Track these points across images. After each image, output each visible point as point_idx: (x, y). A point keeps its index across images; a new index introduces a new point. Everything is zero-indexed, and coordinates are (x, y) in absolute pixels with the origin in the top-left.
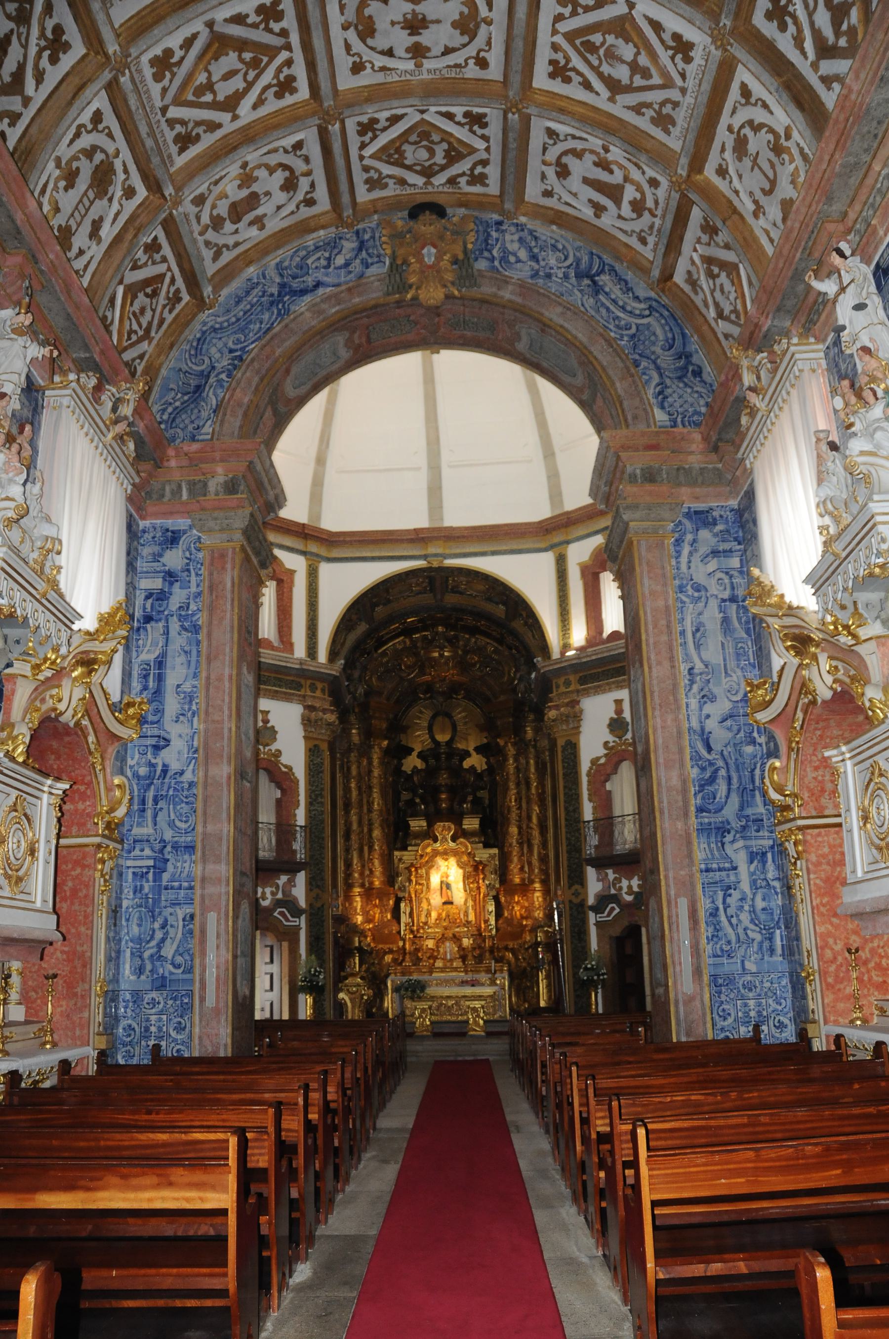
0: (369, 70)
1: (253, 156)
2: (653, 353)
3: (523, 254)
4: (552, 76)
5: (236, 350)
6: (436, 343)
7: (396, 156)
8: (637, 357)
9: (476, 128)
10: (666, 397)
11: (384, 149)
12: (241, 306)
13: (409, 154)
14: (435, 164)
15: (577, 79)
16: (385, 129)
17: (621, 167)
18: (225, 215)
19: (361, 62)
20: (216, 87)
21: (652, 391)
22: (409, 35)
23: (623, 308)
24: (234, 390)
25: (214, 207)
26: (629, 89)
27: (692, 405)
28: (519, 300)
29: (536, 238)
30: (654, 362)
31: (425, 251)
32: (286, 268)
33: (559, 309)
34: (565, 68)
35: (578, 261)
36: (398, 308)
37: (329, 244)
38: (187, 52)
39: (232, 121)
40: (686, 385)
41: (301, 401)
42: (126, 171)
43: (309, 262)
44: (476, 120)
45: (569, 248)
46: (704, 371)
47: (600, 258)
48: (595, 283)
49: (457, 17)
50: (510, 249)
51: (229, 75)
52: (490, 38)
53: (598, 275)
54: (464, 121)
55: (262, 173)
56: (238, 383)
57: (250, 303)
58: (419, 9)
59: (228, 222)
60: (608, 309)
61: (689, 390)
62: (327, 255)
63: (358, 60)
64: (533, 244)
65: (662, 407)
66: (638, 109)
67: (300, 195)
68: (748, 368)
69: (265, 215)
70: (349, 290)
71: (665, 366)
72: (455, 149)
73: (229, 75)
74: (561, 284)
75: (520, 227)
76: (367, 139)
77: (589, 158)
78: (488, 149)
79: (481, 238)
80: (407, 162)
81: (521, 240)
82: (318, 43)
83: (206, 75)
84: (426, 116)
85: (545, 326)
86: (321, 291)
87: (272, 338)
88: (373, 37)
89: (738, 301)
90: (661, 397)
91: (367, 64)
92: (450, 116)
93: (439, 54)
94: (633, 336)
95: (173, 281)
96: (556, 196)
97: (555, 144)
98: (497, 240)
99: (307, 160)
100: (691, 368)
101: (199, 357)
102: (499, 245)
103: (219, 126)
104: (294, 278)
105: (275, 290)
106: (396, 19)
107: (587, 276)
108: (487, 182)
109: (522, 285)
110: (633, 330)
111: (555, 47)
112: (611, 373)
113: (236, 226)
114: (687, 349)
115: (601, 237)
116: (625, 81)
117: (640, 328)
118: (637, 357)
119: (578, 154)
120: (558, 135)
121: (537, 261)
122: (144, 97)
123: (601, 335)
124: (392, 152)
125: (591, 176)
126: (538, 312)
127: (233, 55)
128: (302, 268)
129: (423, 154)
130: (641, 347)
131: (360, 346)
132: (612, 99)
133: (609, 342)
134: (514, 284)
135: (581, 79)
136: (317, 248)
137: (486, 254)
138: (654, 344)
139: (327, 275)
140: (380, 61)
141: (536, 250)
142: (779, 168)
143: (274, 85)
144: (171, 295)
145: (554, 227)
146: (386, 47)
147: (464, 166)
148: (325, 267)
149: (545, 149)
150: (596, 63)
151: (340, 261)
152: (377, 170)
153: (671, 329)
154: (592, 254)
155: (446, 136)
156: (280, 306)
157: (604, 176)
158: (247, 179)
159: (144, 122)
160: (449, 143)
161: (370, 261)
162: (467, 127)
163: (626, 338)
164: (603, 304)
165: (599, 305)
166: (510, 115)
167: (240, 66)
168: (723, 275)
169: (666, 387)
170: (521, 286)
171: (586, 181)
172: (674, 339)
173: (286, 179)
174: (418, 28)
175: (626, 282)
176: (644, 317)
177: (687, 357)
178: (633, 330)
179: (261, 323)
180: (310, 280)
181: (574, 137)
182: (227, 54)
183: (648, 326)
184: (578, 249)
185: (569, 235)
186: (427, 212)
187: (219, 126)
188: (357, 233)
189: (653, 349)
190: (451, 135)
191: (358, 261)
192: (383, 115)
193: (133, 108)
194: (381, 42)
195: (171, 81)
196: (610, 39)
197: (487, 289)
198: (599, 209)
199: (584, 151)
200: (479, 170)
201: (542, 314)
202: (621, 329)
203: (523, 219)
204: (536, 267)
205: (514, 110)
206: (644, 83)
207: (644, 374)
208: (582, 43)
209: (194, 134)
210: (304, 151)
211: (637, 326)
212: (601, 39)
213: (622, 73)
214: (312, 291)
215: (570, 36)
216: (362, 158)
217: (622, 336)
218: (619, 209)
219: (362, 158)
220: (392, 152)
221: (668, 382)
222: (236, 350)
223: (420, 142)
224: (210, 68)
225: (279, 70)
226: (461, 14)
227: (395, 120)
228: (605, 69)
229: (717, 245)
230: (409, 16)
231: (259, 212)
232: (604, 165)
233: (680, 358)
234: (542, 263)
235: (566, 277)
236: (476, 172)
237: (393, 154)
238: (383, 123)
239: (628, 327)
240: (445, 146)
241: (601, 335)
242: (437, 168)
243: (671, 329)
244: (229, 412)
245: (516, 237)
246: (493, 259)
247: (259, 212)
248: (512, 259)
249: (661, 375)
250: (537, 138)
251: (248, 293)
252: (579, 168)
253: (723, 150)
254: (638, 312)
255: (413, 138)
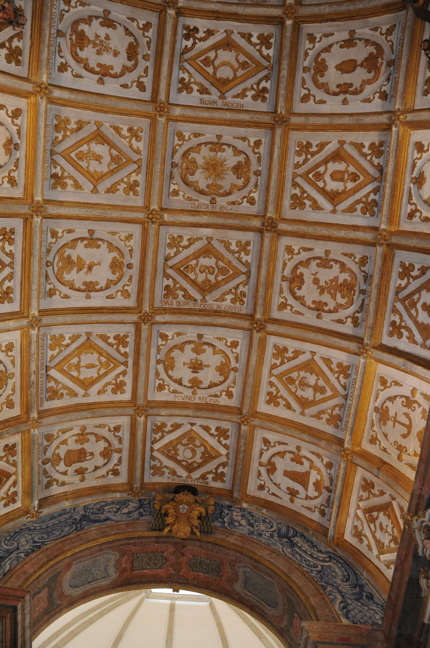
0: (166, 391)
1: (90, 423)
2: (335, 582)
3: (243, 522)
4: (268, 402)
5: (38, 542)
6: (178, 582)
7: (173, 452)
8: (324, 584)
9: (222, 439)
10: (349, 611)
11: (166, 446)
12: (53, 521)
13: (180, 452)
14: (195, 462)
15: (283, 403)
16: (170, 432)
17: (308, 459)
18: (62, 457)
19: (163, 385)
20: (81, 369)
21: (337, 606)
22: (192, 372)
23: (311, 556)
24: (26, 563)
25: (58, 447)
26: (314, 403)
27: (370, 618)
28: (240, 544)
29: (252, 516)
30: (337, 588)
31: (181, 506)
32: (90, 509)
33: (267, 552)
34: (276, 397)
35: (279, 530)
36: (157, 542)
37: (120, 502)
38: (73, 342)
39: (84, 396)
40: (363, 604)
41: (73, 603)
42: (13, 390)
43: (105, 508)
44: (222, 433)
45: (274, 522)
46: (375, 596)
47: (293, 529)
48: (291, 541)
49: (219, 365)
50: (235, 519)
51: (90, 366)
52: (235, 379)
53: (293, 537)
54: (215, 433)
55: (92, 438)
56: (30, 560)
57: (59, 521)
58: (199, 357)
59: (62, 462)
60: (300, 555)
61: (366, 608)
62: (118, 507)
63: (162, 383)
64: (251, 518)
65: (348, 618)
66: (318, 416)
67: (111, 466)
68: (420, 529)
69: (87, 469)
70: (127, 524)
71: (345, 591)
72: (208, 453)
73: (90, 366)
74: (269, 540)
75: (242, 510)
76: (158, 436)
77: (288, 456)
78: (227, 455)
79: (218, 511)
80: (179, 458)
81: (242, 516)
82: (142, 363)
83: (78, 359)
84: (194, 428)
85: (257, 563)
86: (108, 522)
87: (66, 540)
88: (172, 370)
89: (395, 530)
90: (344, 611)
91: (166, 387)
92: (207, 429)
93: (207, 386)
94: (319, 572)
95: (15, 484)
96: (267, 489)
97: (267, 450)
98: (228, 514)
99: (120, 440)
100: (364, 594)
101: (11, 541)
102: (228, 516)
103: (76, 395)
104: (92, 514)
105: (78, 517)
106: (186, 362)
107: (287, 538)
108: (225, 479)
109: (242, 537)
110: (320, 568)
111: (271, 384)
112: (304, 590)
113: (67, 468)
114: (359, 583)
115: (294, 515)
116: (311, 398)
117: (324, 567)
118: (324, 584)
119: (281, 454)
120: (270, 443)
121: (253, 527)
122: (40, 355)
123: (297, 568)
124: (171, 448)
125: (289, 469)
126: (252, 552)
127: (96, 355)
128: (99, 510)
129: (189, 454)
130: (326, 578)
131: (125, 570)
132: (302, 413)
133: (303, 573)
134: (236, 535)
135: (284, 403)
136: (113, 503)
137: (220, 520)
138: (335, 577)
139: (115, 516)
140: (174, 386)
141: (252, 521)
142: (412, 414)
143: (113, 384)
144: (10, 493)
145: (264, 511)
146: (178, 377)
147: (211, 466)
148: (114, 512)
149: (261, 454)
150: (294, 390)
151: (125, 510)
152: (160, 461)
153: (346, 570)
154: (288, 526)
155: (204, 443)
156: (78, 525)
157: (298, 468)
158: (82, 437)
159: (35, 363)
160: (205, 448)
161: (144, 513)
162: (217, 438)
163: (314, 572)
164: (297, 552)
165: (294, 553)
166: (243, 427)
167: (98, 363)
168: (381, 514)
169: (348, 604)
170: (241, 537)
171: (286, 474)
172: (349, 575)
173: (105, 448)
174: (197, 369)
175: (312, 543)
176: (326, 562)
177: (360, 587)
178: (320, 568)
179: (62, 531)
180: (103, 517)
181: (280, 443)
182: (92, 354)
183: (330, 567)
184: (280, 524)
185: (274, 515)
186: (186, 491)
187: (76, 395)
188: (140, 500)
189: (335, 580)
190: (207, 442)
191: (137, 512)
192: (169, 422)
193: (32, 352)
194: (175, 374)
195: (58, 354)
196: (302, 374)
197: (218, 536)
198: (293, 493)
199: (285, 452)
200: (221, 470)
201: (255, 553)
202: (311, 567)
203: (245, 505)
204: (252, 529)
205: (246, 423)
206: (322, 396)
207: (330, 594)
208: (286, 379)
209: (60, 392)
210: (120, 434)
211: (322, 566)
212: (297, 374)
213: (309, 394)
214: (102, 521)
215: (279, 377)
216: (152, 450)
217: (312, 571)
218: (307, 490)
219: (152, 450)
220: (171, 448)
221: (349, 601)
222: (38, 542)
223: (188, 445)
224: (81, 356)
225: (118, 376)
226: (222, 362)
227: (176, 427)
228: (300, 393)
229: (375, 495)
230: (194, 361)
231: (84, 465)
232: (297, 459)
233: (355, 587)
234: (256, 528)
235: (272, 536)
236: (219, 471)
237: (170, 451)
238: (169, 428)
239: (316, 566)
240: (202, 449)
241: (297, 568)
242: (196, 465)
243: (346, 570)
244: (15, 576)
245: (240, 514)
246: (224, 522)
247: (84, 465)
248: (237, 524)
249: (343, 596)
250: (258, 445)
251: (60, 515)
252: (282, 464)
253: (372, 425)
254: (321, 559)
255: (185, 441)
